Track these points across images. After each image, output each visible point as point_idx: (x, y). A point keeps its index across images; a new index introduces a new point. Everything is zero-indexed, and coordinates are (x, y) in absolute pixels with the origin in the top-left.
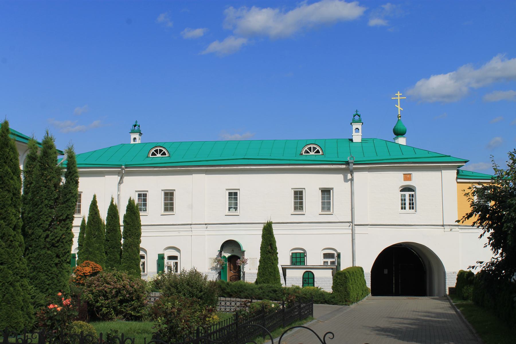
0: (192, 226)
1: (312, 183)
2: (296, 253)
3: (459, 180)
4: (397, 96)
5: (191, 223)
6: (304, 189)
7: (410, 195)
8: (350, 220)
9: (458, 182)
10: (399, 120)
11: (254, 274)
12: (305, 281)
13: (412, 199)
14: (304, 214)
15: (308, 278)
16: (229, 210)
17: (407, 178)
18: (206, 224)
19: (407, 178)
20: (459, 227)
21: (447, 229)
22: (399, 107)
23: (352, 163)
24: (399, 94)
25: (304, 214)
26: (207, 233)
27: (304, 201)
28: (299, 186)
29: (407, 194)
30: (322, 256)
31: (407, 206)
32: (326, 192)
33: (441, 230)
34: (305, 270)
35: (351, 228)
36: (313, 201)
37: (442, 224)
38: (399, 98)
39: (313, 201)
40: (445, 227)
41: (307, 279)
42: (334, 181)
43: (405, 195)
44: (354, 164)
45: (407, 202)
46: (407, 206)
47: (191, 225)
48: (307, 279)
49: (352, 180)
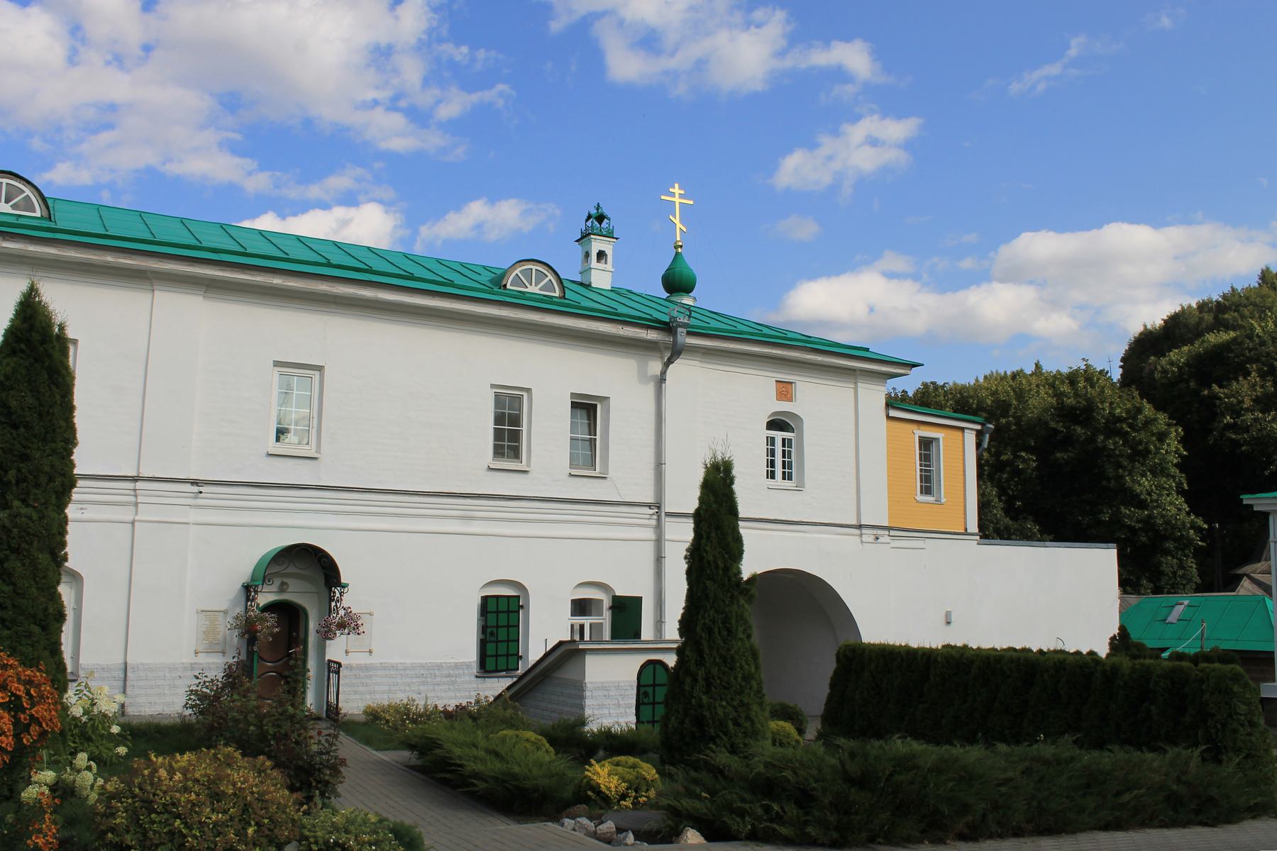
0: (139, 485)
1: (552, 374)
2: (497, 597)
3: (893, 413)
4: (673, 195)
5: (132, 473)
6: (528, 390)
7: (784, 440)
8: (650, 500)
9: (888, 417)
10: (677, 254)
11: (468, 666)
12: (646, 694)
13: (790, 452)
14: (525, 472)
15: (654, 685)
16: (278, 439)
17: (785, 390)
18: (195, 483)
19: (785, 390)
20: (892, 533)
21: (868, 535)
22: (677, 221)
23: (685, 325)
24: (676, 190)
25: (525, 472)
26: (194, 516)
27: (524, 428)
28: (512, 379)
29: (779, 435)
30: (568, 608)
31: (779, 470)
32: (586, 408)
33: (849, 541)
34: (643, 659)
35: (654, 522)
36: (548, 430)
37: (854, 522)
38: (677, 200)
39: (548, 430)
40: (864, 531)
41: (650, 690)
42: (614, 377)
43: (773, 439)
44: (689, 333)
45: (779, 460)
46: (779, 470)
47: (135, 479)
48: (650, 690)
49: (662, 379)
